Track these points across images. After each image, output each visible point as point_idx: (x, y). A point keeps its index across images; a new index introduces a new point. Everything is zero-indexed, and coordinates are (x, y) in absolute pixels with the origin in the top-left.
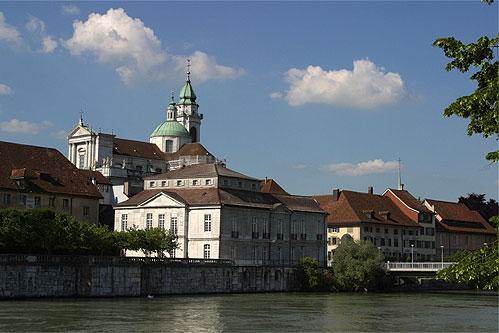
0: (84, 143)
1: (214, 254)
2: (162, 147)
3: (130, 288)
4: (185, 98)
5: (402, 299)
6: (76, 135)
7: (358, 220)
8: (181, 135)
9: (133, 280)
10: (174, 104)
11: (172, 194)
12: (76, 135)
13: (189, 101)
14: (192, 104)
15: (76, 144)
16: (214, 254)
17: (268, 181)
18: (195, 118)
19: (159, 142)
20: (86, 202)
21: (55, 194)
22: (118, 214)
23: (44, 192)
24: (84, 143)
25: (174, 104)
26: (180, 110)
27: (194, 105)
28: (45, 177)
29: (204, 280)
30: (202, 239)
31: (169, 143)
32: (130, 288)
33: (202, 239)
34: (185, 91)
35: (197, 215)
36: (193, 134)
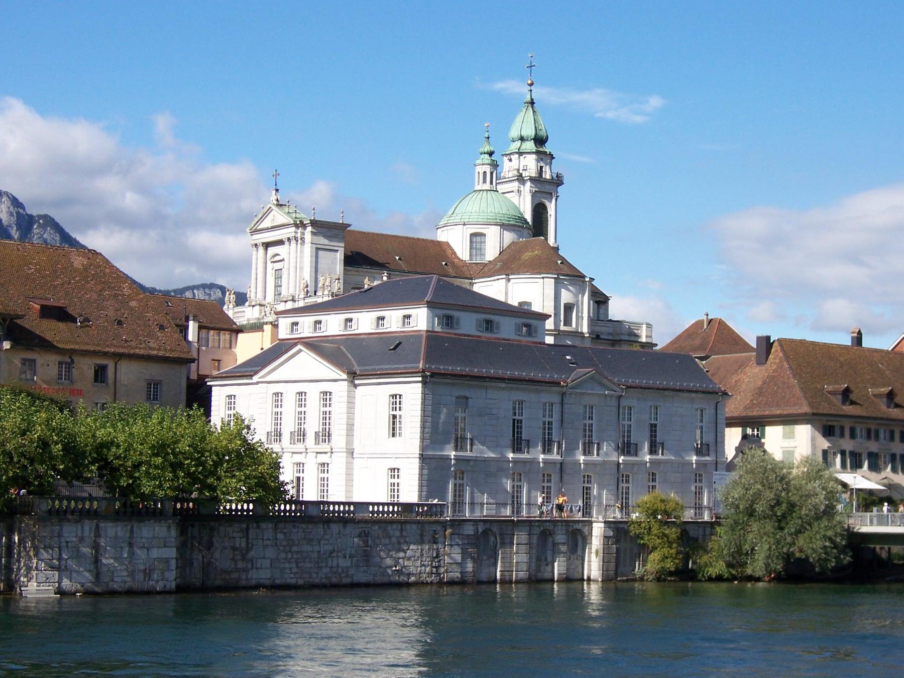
0: (280, 242)
1: (410, 494)
2: (462, 251)
3: (148, 573)
4: (522, 139)
5: (368, 619)
6: (266, 224)
7: (806, 409)
8: (514, 224)
9: (155, 553)
10: (491, 154)
11: (316, 346)
12: (266, 224)
13: (530, 146)
14: (537, 153)
15: (267, 245)
16: (410, 494)
17: (710, 321)
18: (546, 187)
19: (457, 241)
20: (154, 371)
21: (72, 352)
22: (219, 395)
23: (46, 346)
24: (280, 242)
25: (491, 154)
26: (509, 167)
27: (544, 157)
28: (48, 312)
29: (366, 557)
30: (384, 456)
31: (476, 238)
32: (148, 573)
33: (384, 456)
34: (524, 124)
35: (374, 396)
36: (539, 224)
